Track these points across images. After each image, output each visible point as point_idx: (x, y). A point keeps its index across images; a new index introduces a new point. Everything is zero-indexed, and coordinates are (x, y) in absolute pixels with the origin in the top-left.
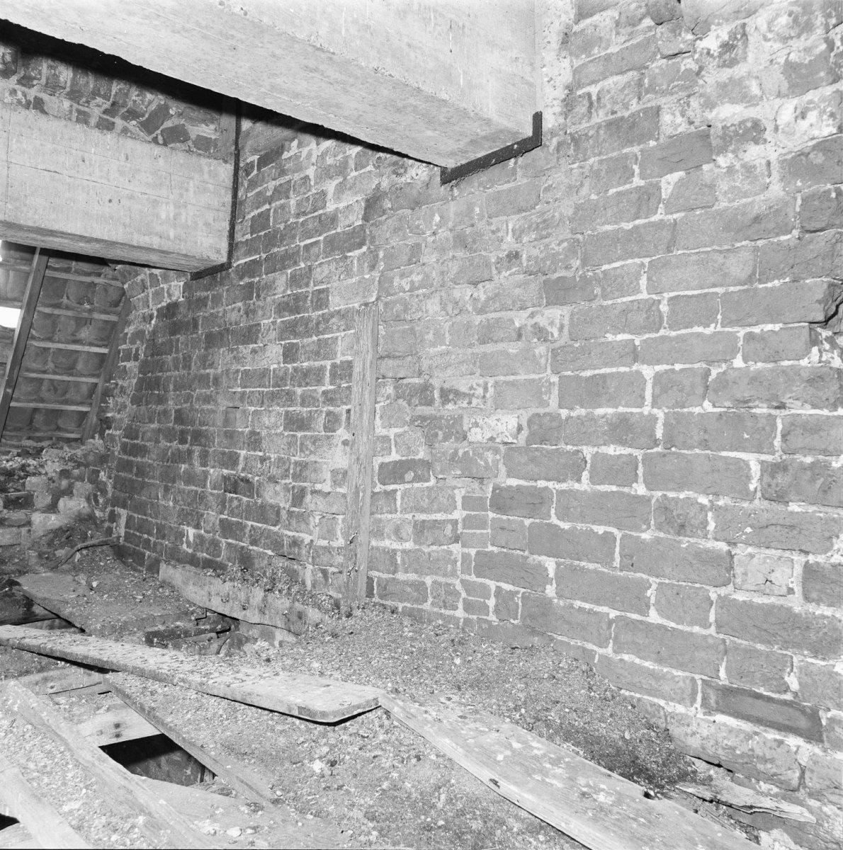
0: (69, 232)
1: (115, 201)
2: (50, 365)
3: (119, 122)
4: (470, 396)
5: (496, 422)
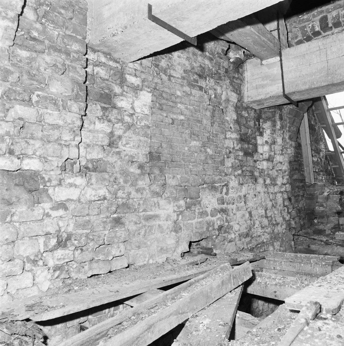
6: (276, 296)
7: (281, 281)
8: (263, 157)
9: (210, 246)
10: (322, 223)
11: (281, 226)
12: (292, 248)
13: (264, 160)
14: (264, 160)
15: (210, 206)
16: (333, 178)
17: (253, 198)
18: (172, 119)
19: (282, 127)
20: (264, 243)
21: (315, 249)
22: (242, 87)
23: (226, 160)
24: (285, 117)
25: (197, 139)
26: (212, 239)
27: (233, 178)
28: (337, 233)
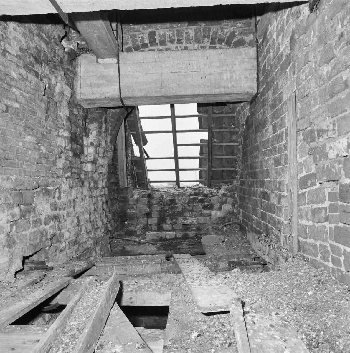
0: (186, 94)
1: (204, 77)
2: (224, 153)
3: (217, 46)
4: (328, 131)
5: (338, 144)
6: (131, 303)
7: (135, 287)
8: (87, 159)
9: (43, 258)
10: (132, 224)
11: (101, 230)
12: (109, 251)
13: (88, 162)
14: (88, 162)
15: (44, 213)
16: (136, 182)
17: (80, 202)
18: (6, 105)
19: (107, 130)
20: (88, 249)
21: (129, 250)
22: (74, 82)
23: (58, 160)
24: (110, 119)
25: (31, 133)
26: (45, 251)
27: (65, 180)
28: (147, 233)
